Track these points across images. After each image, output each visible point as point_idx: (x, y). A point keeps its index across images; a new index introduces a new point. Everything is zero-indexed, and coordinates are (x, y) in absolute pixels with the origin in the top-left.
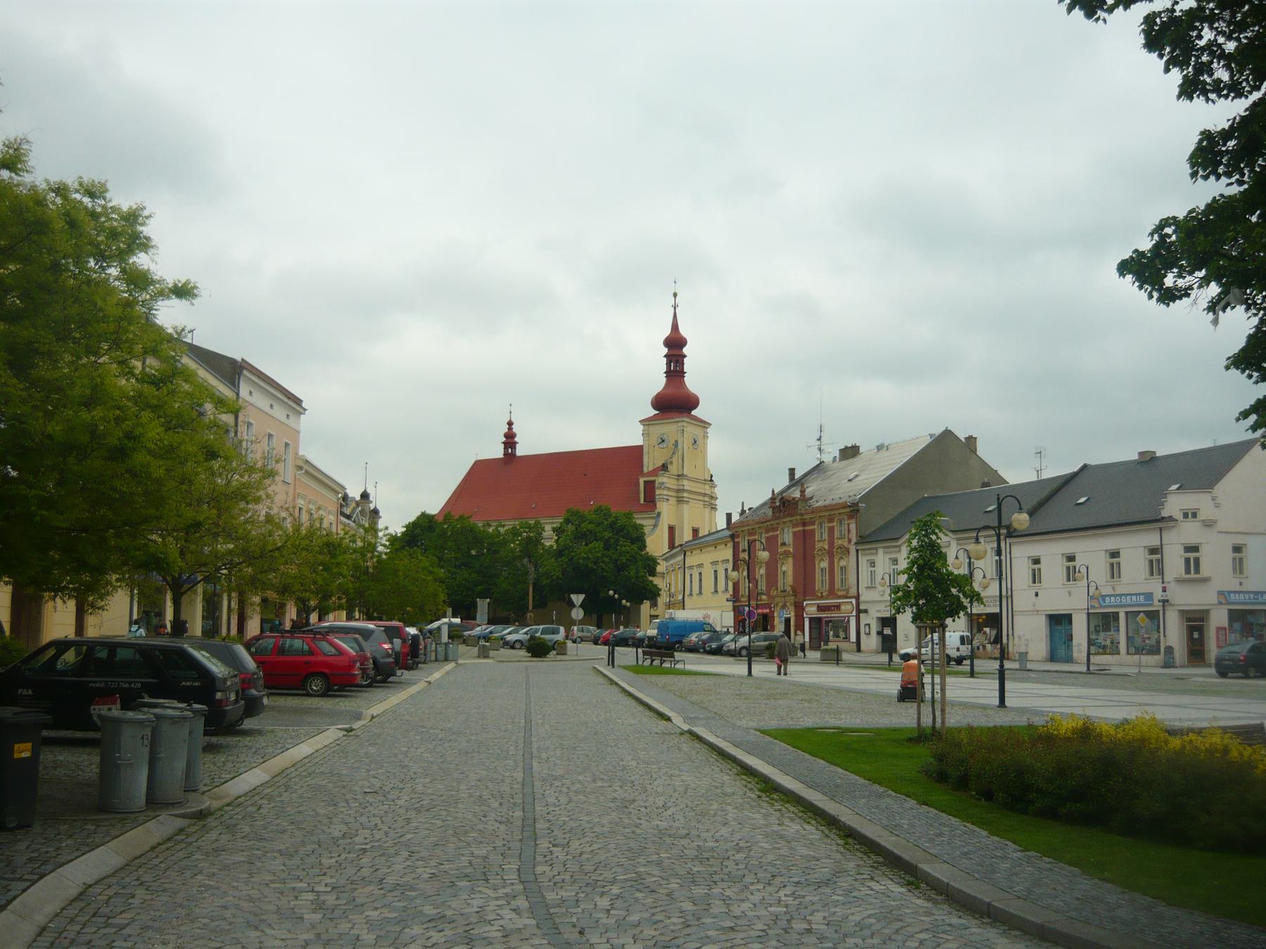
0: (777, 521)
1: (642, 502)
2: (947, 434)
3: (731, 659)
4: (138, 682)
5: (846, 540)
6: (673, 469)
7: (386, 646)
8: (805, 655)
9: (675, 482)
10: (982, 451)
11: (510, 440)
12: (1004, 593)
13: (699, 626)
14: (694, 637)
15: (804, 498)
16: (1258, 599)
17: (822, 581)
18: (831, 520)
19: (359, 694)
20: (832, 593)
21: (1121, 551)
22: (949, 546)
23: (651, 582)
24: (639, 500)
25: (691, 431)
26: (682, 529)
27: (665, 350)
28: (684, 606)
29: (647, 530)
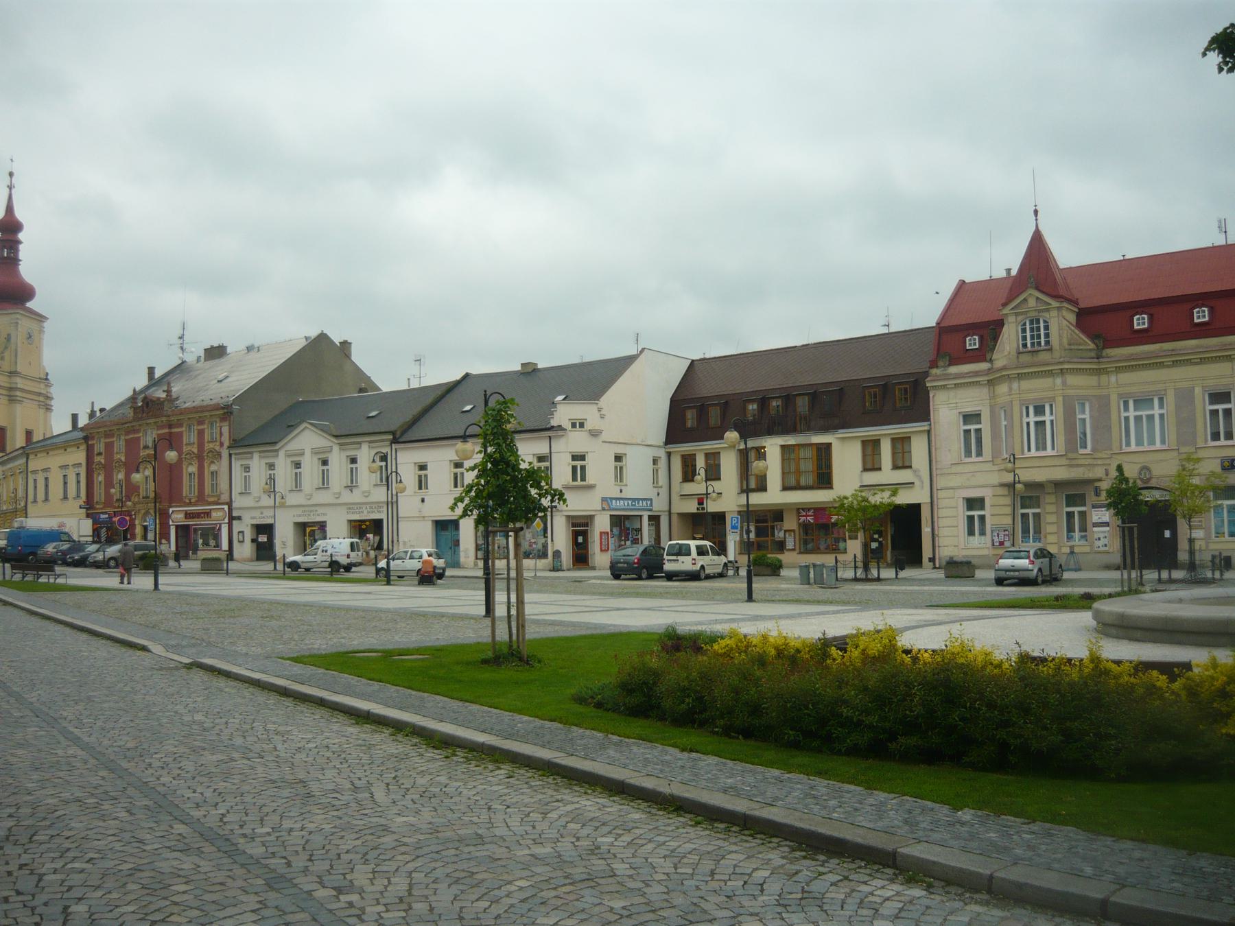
0: (140, 423)
2: (323, 337)
3: (100, 571)
5: (218, 444)
8: (180, 565)
9: (6, 379)
10: (358, 357)
12: (390, 500)
13: (55, 536)
14: (50, 548)
15: (170, 399)
16: (635, 505)
17: (190, 486)
18: (200, 423)
20: (201, 499)
21: (429, 464)
25: (25, 324)
28: (26, 513)
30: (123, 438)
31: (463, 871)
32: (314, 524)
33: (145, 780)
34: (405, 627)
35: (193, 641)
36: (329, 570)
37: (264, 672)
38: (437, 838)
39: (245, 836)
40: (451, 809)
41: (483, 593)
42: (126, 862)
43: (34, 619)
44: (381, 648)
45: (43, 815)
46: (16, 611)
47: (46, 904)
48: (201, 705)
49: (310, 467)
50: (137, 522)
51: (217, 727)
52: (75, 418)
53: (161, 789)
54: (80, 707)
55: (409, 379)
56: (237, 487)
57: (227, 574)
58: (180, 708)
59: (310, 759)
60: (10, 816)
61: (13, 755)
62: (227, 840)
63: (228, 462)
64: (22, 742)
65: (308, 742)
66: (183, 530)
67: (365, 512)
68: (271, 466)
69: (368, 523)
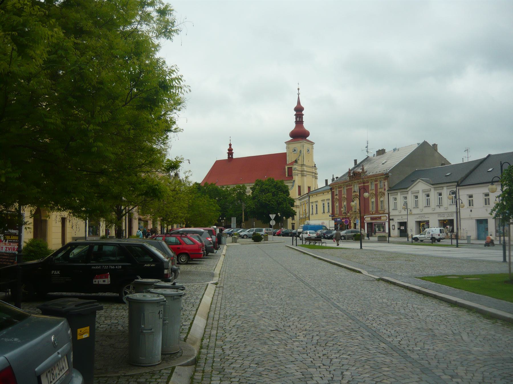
0: (352, 182)
1: (287, 176)
2: (425, 143)
4: (120, 265)
5: (383, 189)
6: (300, 162)
7: (209, 239)
8: (369, 239)
9: (300, 167)
11: (230, 152)
15: (364, 172)
18: (376, 181)
19: (202, 262)
20: (377, 212)
22: (430, 191)
23: (292, 209)
24: (285, 175)
25: (307, 146)
26: (304, 187)
27: (295, 113)
28: (309, 219)
29: (289, 187)
30: (345, 188)
31: (506, 373)
32: (424, 221)
33: (367, 325)
34: (467, 266)
35: (379, 270)
36: (431, 241)
37: (410, 283)
38: (493, 358)
39: (410, 350)
40: (498, 346)
41: (502, 251)
42: (363, 357)
43: (316, 259)
44: (458, 274)
45: (329, 336)
46: (308, 256)
47: (334, 370)
48: (385, 296)
49: (422, 198)
50: (351, 222)
51: (393, 305)
52: (327, 181)
53: (374, 329)
54: (338, 294)
55: (463, 159)
56: (392, 207)
57: (389, 242)
58: (377, 296)
59: (433, 320)
60: (317, 335)
61: (315, 312)
62: (403, 351)
64: (318, 307)
65: (431, 313)
66: (370, 225)
67: (446, 216)
68: (406, 198)
69: (447, 221)
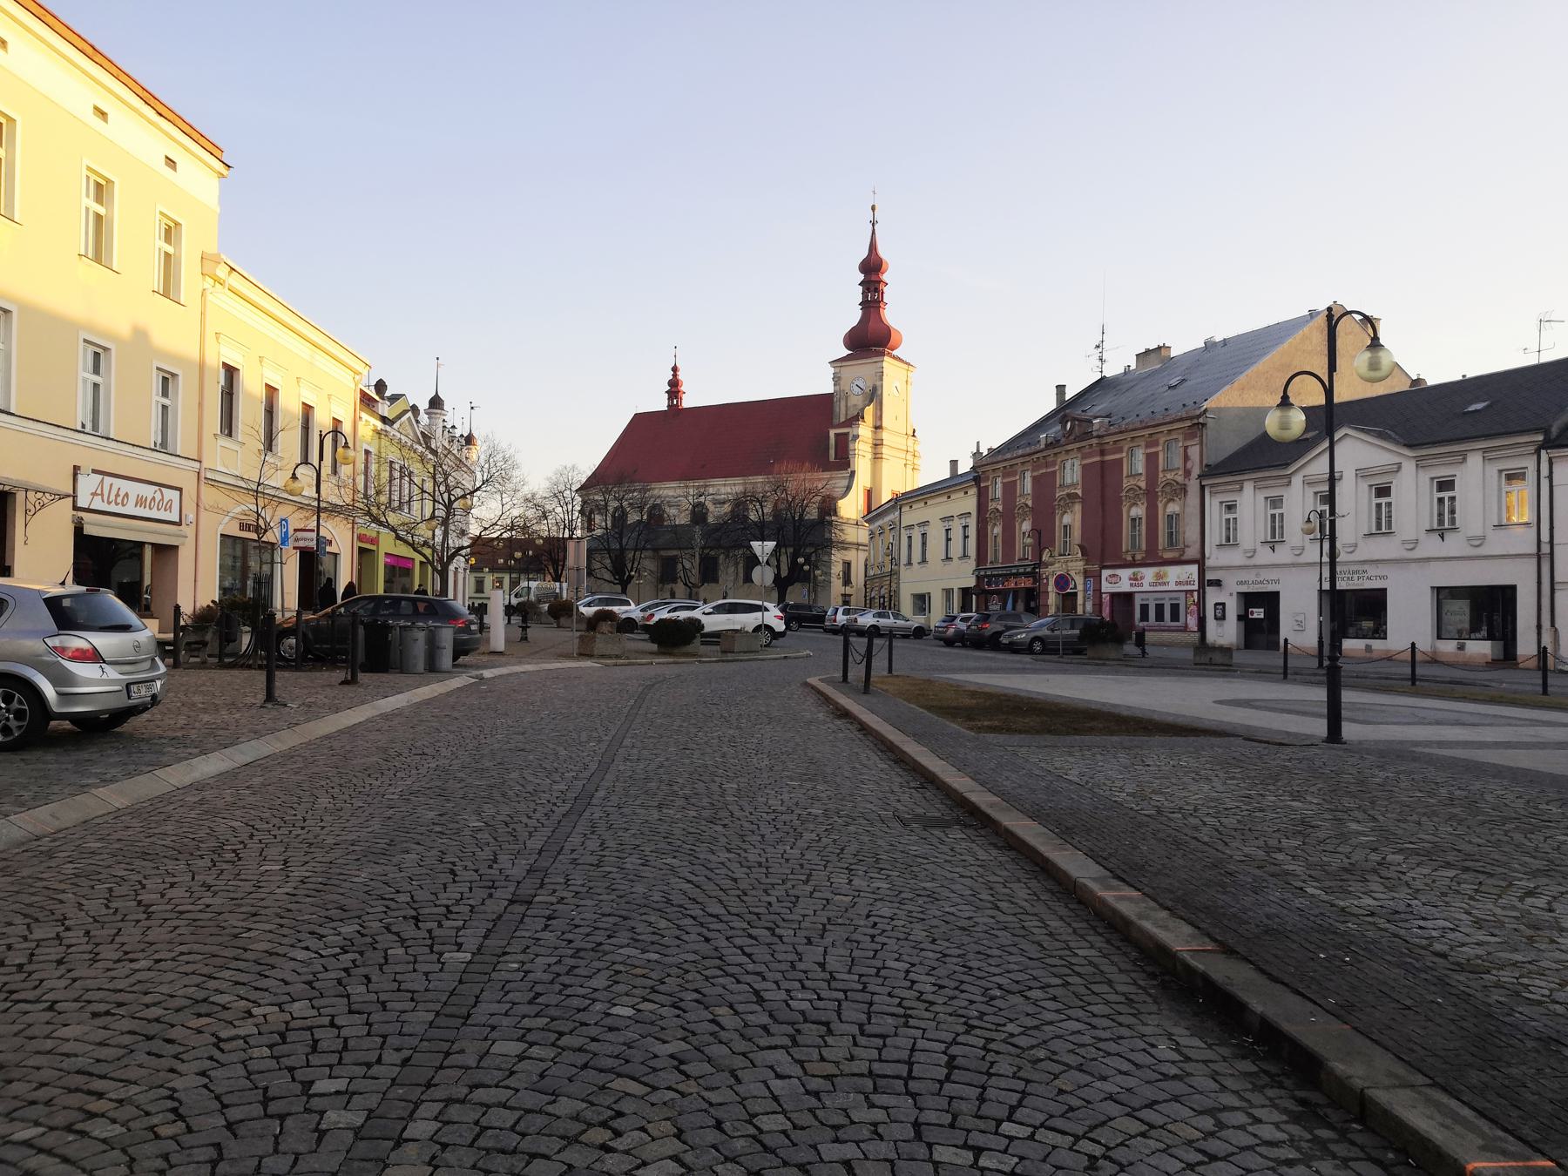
0: (1056, 450)
8: (1144, 652)
11: (674, 389)
27: (862, 277)
52: (954, 463)
63: (1197, 501)
68: (1276, 502)
